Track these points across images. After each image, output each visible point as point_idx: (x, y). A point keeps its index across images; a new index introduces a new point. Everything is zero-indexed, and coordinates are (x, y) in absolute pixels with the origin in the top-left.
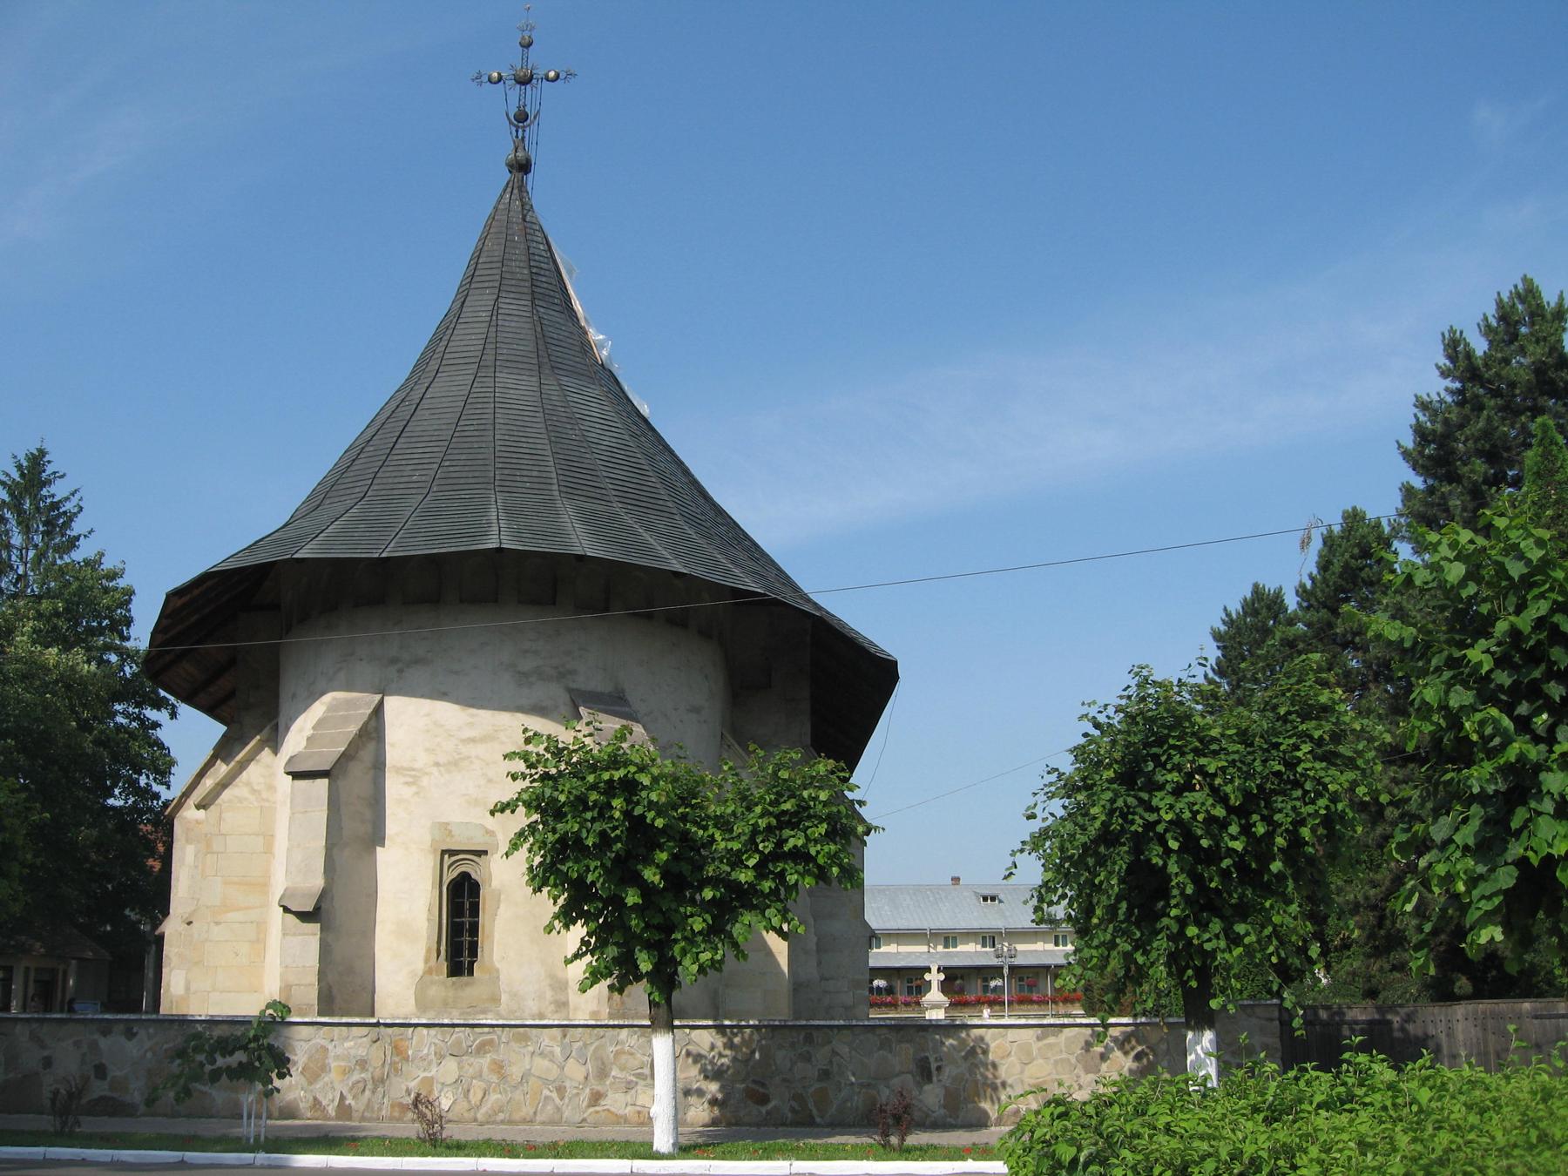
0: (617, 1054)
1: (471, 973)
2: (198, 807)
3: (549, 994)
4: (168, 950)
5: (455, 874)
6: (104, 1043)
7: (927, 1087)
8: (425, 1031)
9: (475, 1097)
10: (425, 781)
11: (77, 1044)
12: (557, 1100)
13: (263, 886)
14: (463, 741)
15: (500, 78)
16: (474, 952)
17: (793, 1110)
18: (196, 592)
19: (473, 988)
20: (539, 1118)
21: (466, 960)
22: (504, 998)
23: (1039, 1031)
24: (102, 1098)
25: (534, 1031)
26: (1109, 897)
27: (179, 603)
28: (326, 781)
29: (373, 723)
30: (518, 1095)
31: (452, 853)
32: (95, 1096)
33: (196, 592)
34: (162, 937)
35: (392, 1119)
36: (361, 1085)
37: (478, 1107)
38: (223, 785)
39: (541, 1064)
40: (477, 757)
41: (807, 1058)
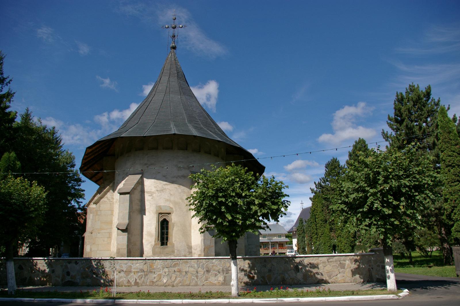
0: (213, 266)
1: (167, 244)
2: (94, 203)
3: (187, 250)
4: (86, 240)
5: (162, 219)
6: (69, 265)
7: (298, 274)
8: (159, 261)
9: (173, 279)
10: (154, 195)
11: (62, 266)
12: (196, 280)
13: (111, 223)
14: (164, 185)
15: (168, 27)
16: (167, 239)
17: (261, 281)
18: (94, 148)
19: (168, 248)
20: (191, 284)
21: (165, 241)
22: (176, 251)
23: (328, 257)
24: (68, 281)
25: (189, 260)
26: (447, 211)
27: (90, 150)
28: (129, 195)
29: (141, 180)
30: (185, 278)
31: (161, 213)
32: (66, 281)
33: (94, 148)
34: (84, 238)
35: (150, 285)
36: (141, 276)
37: (174, 282)
38: (101, 198)
39: (191, 269)
40: (168, 189)
41: (265, 266)
